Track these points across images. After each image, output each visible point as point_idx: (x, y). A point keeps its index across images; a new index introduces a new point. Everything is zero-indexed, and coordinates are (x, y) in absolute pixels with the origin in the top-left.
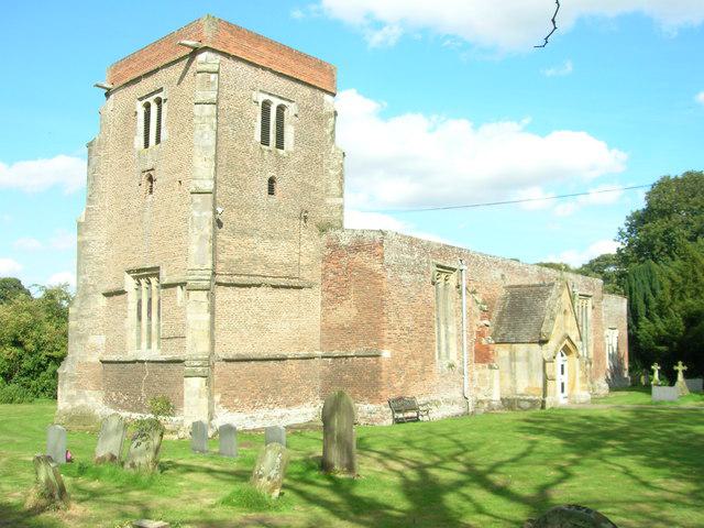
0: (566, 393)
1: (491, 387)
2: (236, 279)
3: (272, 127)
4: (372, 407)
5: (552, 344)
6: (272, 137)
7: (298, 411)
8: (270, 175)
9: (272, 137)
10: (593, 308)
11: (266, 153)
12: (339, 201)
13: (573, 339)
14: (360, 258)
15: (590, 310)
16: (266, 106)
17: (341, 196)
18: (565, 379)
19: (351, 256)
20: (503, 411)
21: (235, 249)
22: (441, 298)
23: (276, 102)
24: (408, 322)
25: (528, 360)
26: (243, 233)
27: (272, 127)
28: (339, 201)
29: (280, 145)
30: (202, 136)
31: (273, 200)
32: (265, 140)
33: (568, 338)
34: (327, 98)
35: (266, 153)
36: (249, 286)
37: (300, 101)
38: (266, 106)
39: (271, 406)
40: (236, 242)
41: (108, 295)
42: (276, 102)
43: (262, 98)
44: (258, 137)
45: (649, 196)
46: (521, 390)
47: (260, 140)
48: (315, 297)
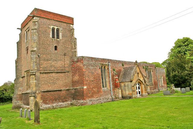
0: (141, 94)
1: (119, 94)
2: (46, 72)
3: (56, 33)
4: (82, 101)
5: (134, 82)
6: (56, 36)
7: (66, 103)
8: (55, 45)
9: (56, 36)
10: (152, 71)
11: (53, 40)
12: (74, 50)
13: (141, 80)
14: (78, 64)
15: (152, 72)
16: (53, 29)
17: (75, 49)
18: (140, 90)
19: (77, 63)
20: (13, 110)
21: (45, 64)
22: (103, 71)
23: (56, 28)
24: (92, 79)
25: (128, 86)
26: (47, 60)
27: (56, 33)
28: (74, 50)
29: (58, 37)
30: (34, 37)
31: (56, 51)
32: (53, 37)
33: (140, 80)
34: (71, 25)
35: (53, 40)
36: (50, 73)
37: (63, 27)
38: (53, 29)
39: (58, 102)
40: (46, 62)
41: (22, 78)
42: (56, 28)
43: (51, 27)
44: (51, 36)
45: (175, 43)
46: (127, 94)
47: (52, 37)
48: (70, 74)
